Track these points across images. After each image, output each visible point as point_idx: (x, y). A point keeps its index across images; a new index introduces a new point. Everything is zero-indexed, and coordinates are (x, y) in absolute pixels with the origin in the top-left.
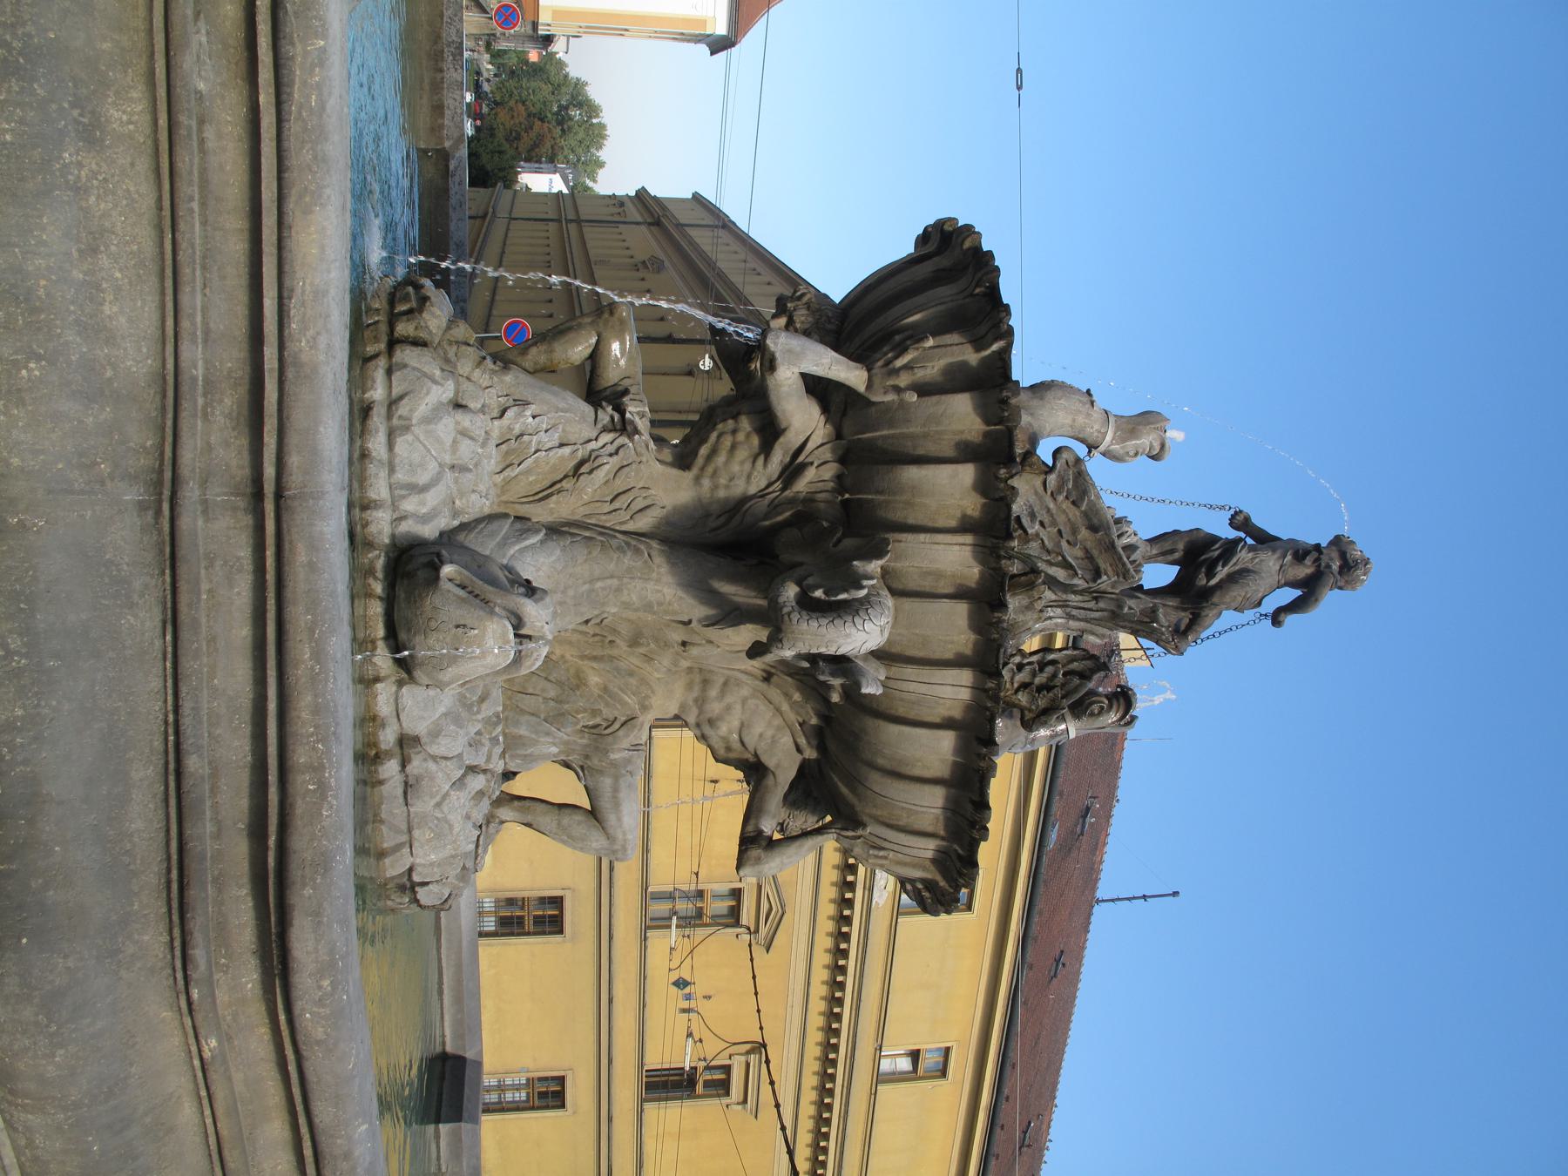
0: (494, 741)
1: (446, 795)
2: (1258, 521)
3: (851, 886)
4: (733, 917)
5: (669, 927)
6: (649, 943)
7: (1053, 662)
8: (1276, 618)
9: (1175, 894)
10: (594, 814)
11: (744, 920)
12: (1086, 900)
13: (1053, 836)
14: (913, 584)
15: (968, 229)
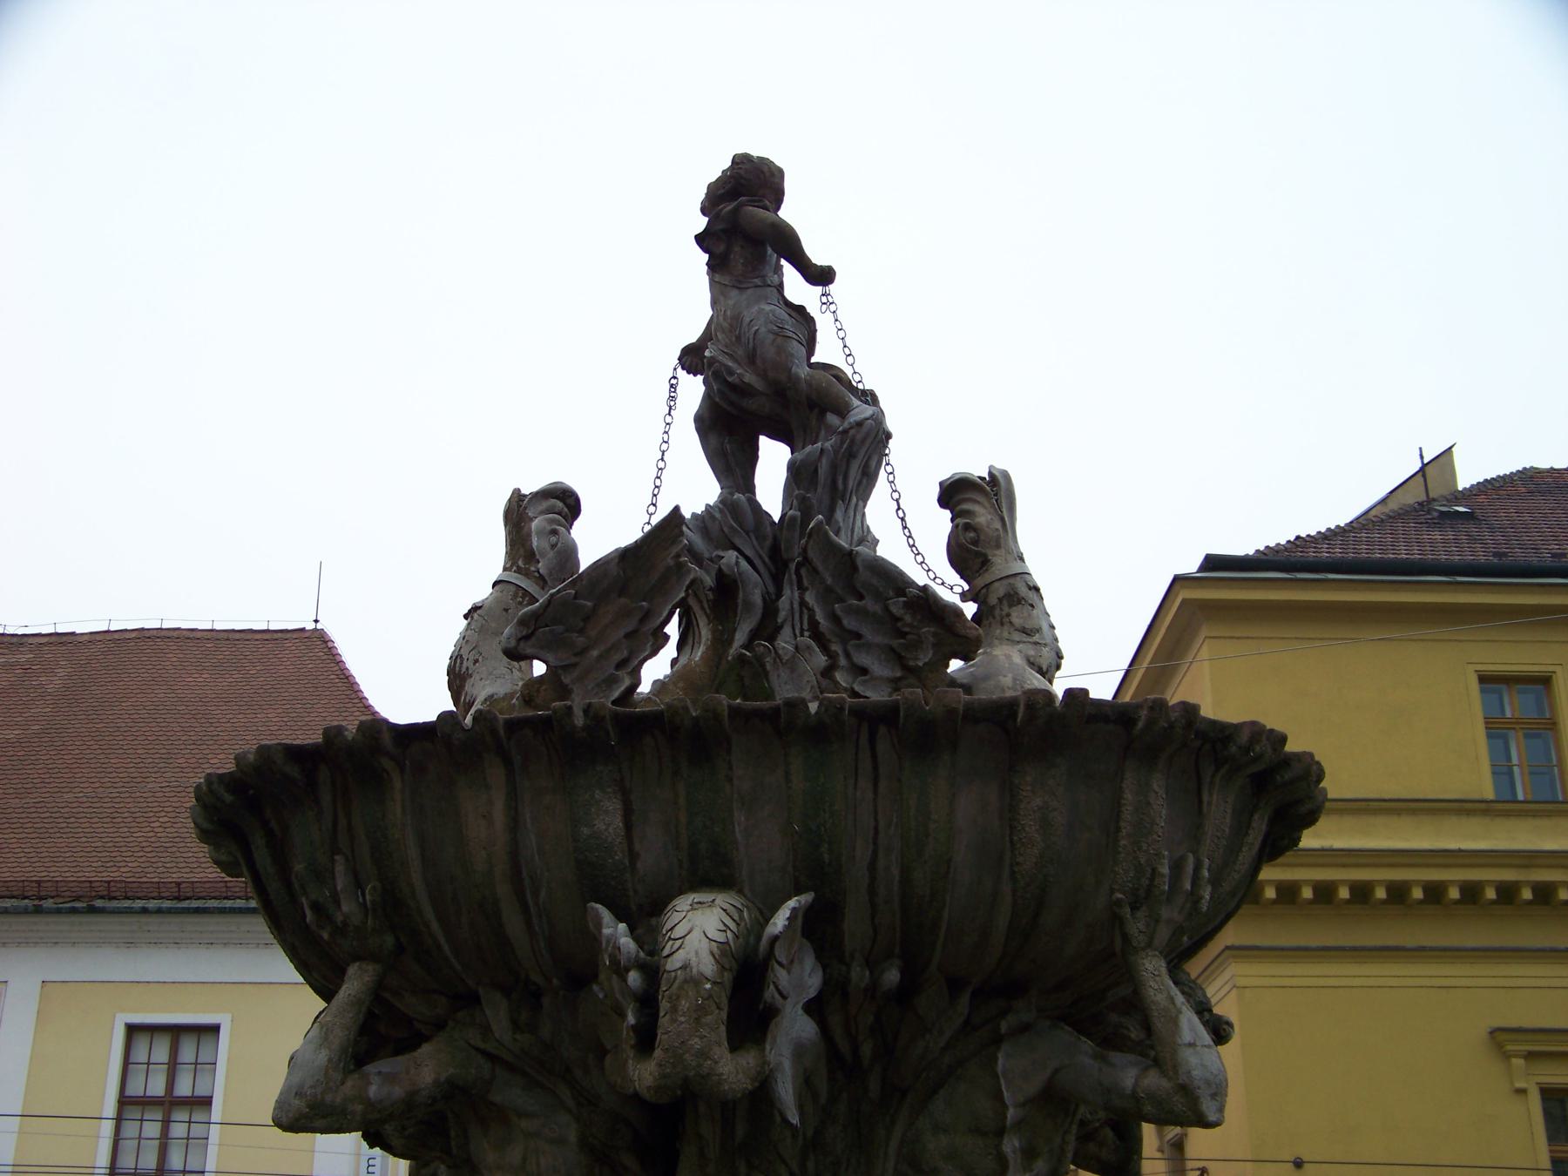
8: (821, 276)
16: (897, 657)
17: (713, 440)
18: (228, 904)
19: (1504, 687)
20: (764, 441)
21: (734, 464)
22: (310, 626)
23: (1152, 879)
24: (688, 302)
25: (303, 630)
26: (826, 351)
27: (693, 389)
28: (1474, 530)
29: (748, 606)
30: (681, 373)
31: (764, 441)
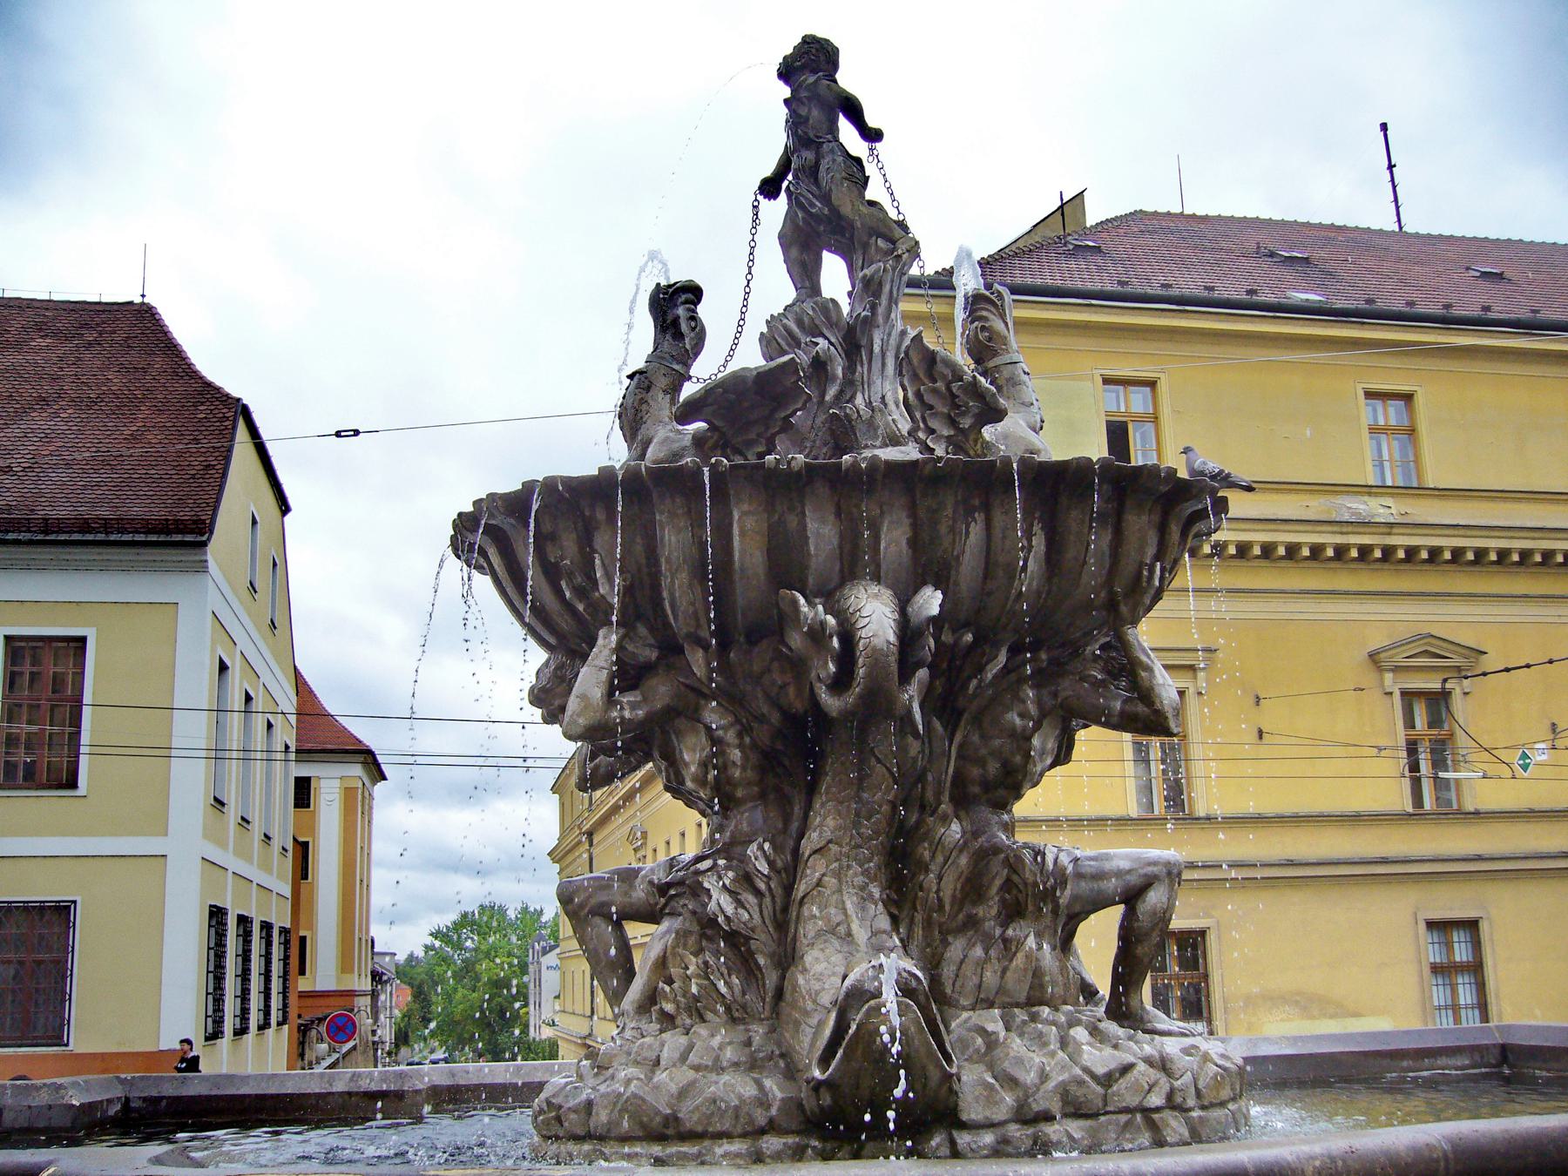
0: (1034, 1018)
1: (1086, 1070)
2: (768, 169)
3: (1388, 552)
4: (1438, 701)
5: (1457, 780)
6: (1483, 807)
7: (918, 395)
8: (872, 136)
9: (1384, 127)
10: (1131, 897)
11: (1435, 685)
12: (1400, 247)
13: (1300, 296)
14: (361, 758)
15: (460, 515)
16: (953, 423)
17: (794, 252)
18: (90, 537)
19: (1121, 388)
20: (826, 255)
21: (805, 274)
22: (138, 300)
23: (689, 511)
24: (768, 142)
25: (131, 303)
26: (874, 192)
27: (776, 210)
28: (1099, 260)
29: (835, 378)
30: (760, 198)
31: (826, 255)
